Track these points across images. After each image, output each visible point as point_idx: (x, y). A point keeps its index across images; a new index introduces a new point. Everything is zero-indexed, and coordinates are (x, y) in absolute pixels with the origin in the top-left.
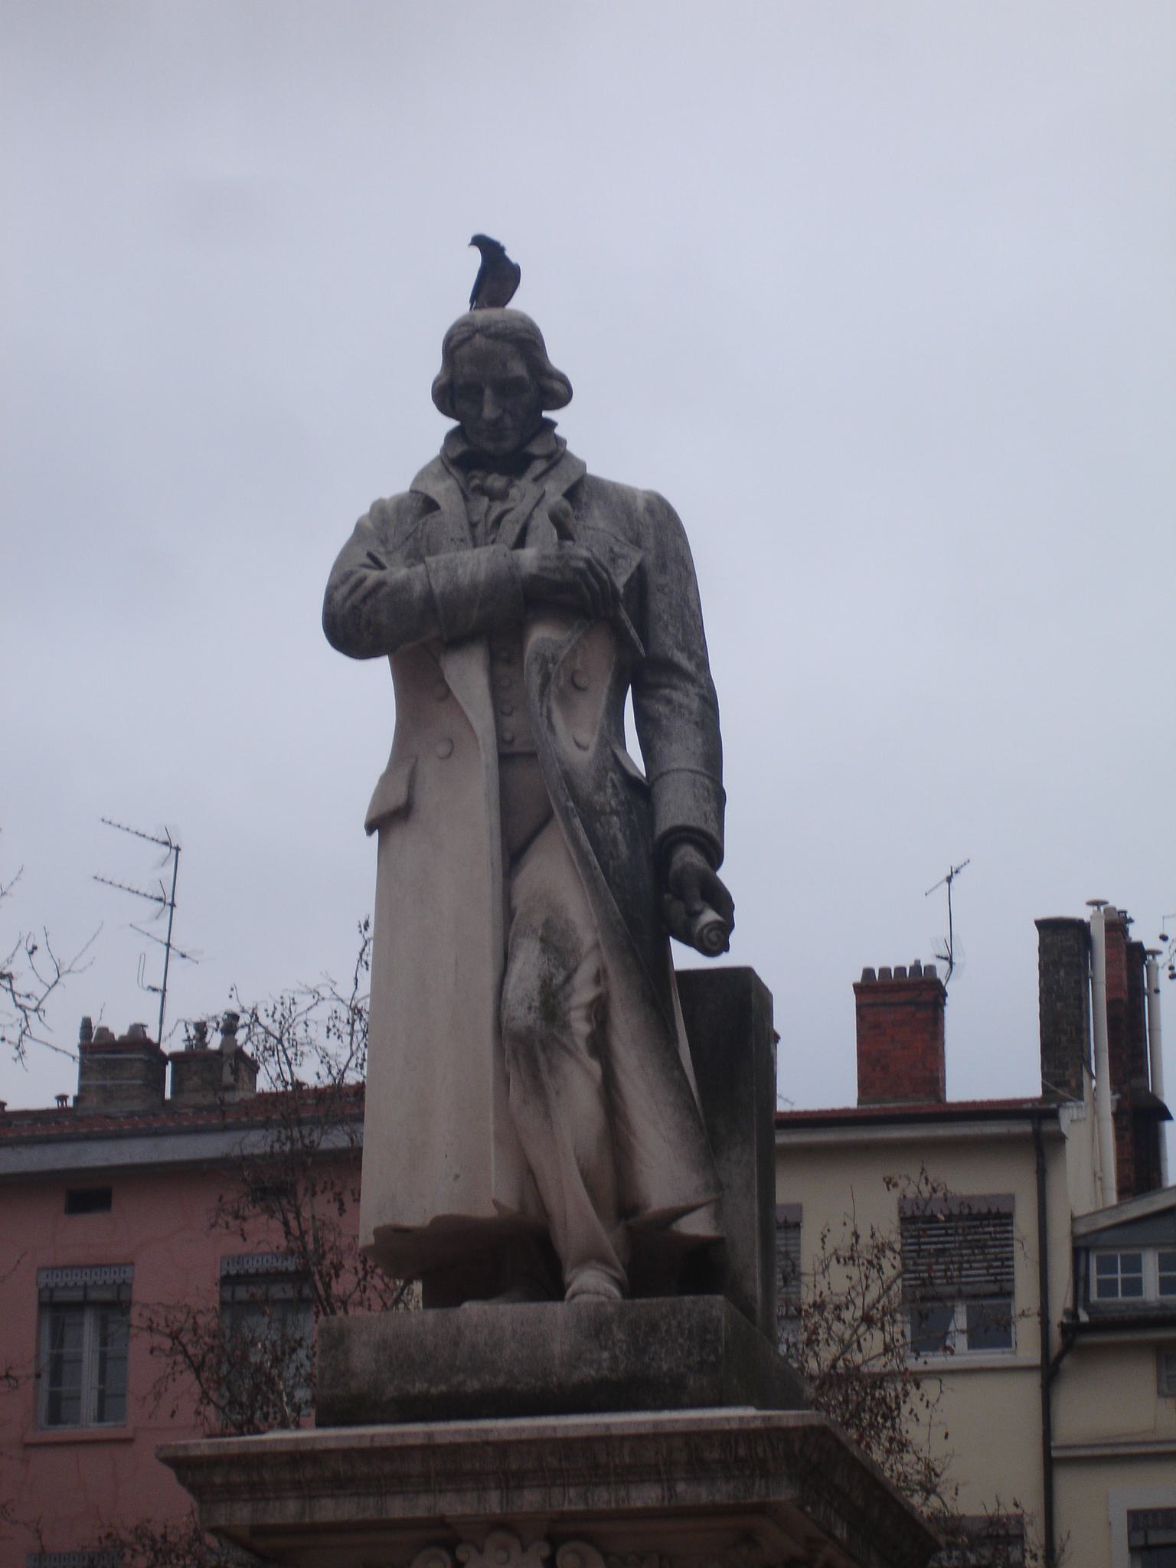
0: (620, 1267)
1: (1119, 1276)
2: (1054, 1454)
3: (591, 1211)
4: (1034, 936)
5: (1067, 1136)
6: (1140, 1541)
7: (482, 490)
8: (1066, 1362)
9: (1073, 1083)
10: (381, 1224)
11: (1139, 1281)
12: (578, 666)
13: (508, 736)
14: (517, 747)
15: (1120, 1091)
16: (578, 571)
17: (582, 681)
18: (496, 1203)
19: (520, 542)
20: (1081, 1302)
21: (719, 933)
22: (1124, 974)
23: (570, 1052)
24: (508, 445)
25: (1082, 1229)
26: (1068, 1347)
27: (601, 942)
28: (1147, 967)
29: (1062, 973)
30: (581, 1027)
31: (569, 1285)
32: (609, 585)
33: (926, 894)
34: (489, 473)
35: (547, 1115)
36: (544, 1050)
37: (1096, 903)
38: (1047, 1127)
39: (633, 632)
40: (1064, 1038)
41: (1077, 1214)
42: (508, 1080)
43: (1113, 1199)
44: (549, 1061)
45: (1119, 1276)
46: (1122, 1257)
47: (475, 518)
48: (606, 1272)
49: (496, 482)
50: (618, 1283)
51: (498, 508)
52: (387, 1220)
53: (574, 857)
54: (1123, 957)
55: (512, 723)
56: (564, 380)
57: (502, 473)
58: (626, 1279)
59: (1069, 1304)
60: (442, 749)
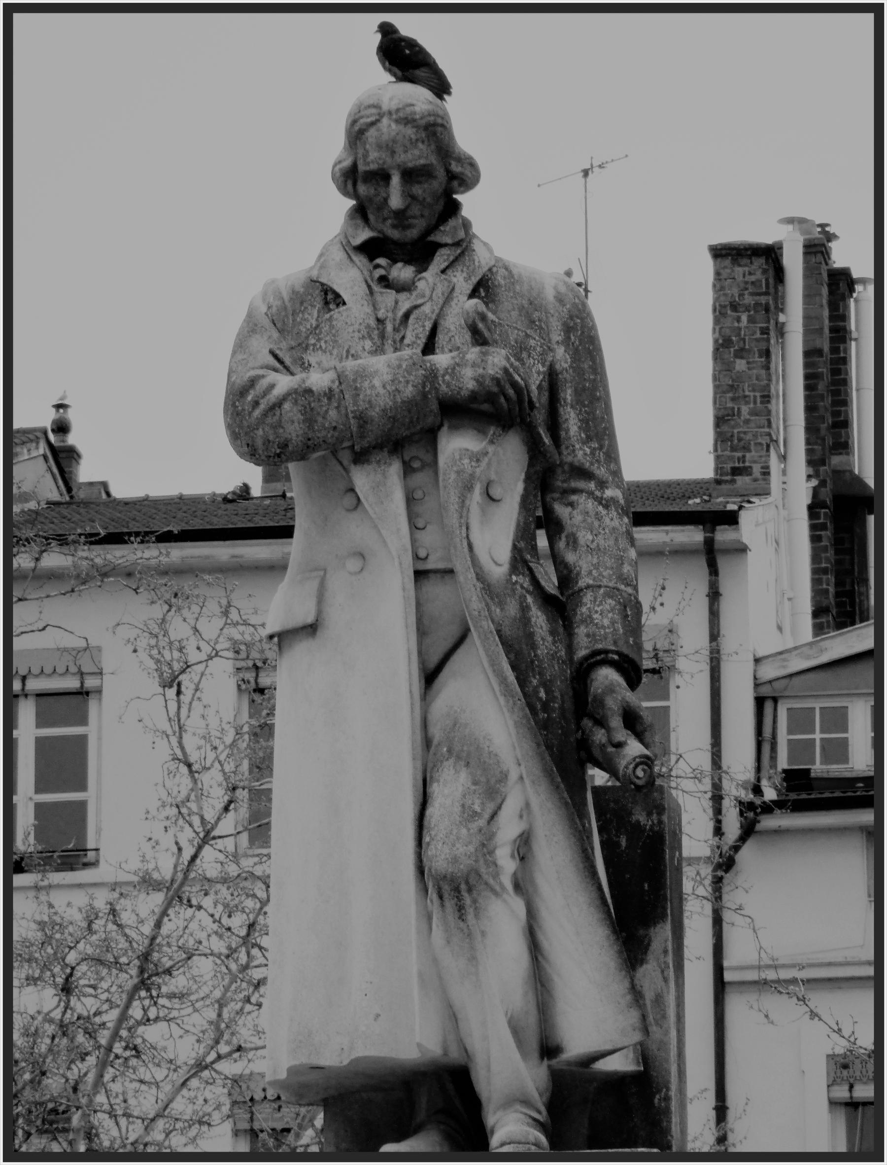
0: (543, 1109)
1: (818, 736)
2: (728, 976)
3: (517, 1055)
4: (708, 265)
5: (750, 547)
6: (842, 1093)
7: (384, 281)
8: (747, 855)
9: (757, 470)
10: (297, 1063)
11: (844, 744)
12: (493, 477)
13: (422, 553)
14: (430, 565)
15: (816, 475)
16: (497, 381)
17: (496, 492)
18: (419, 1045)
19: (429, 348)
20: (764, 773)
21: (646, 767)
22: (826, 313)
23: (496, 894)
24: (413, 234)
25: (769, 672)
26: (748, 831)
27: (525, 776)
28: (856, 301)
29: (744, 318)
30: (508, 865)
31: (492, 1132)
32: (527, 399)
33: (539, 186)
34: (395, 261)
35: (473, 959)
36: (470, 890)
37: (790, 221)
38: (724, 535)
39: (547, 440)
40: (745, 410)
41: (760, 654)
42: (430, 918)
43: (806, 631)
44: (475, 901)
45: (818, 736)
46: (821, 708)
47: (381, 314)
48: (526, 1114)
49: (402, 272)
50: (541, 1126)
51: (405, 302)
52: (303, 1059)
53: (497, 688)
54: (825, 291)
55: (430, 538)
56: (473, 165)
57: (408, 262)
58: (549, 1121)
59: (749, 775)
60: (353, 565)
